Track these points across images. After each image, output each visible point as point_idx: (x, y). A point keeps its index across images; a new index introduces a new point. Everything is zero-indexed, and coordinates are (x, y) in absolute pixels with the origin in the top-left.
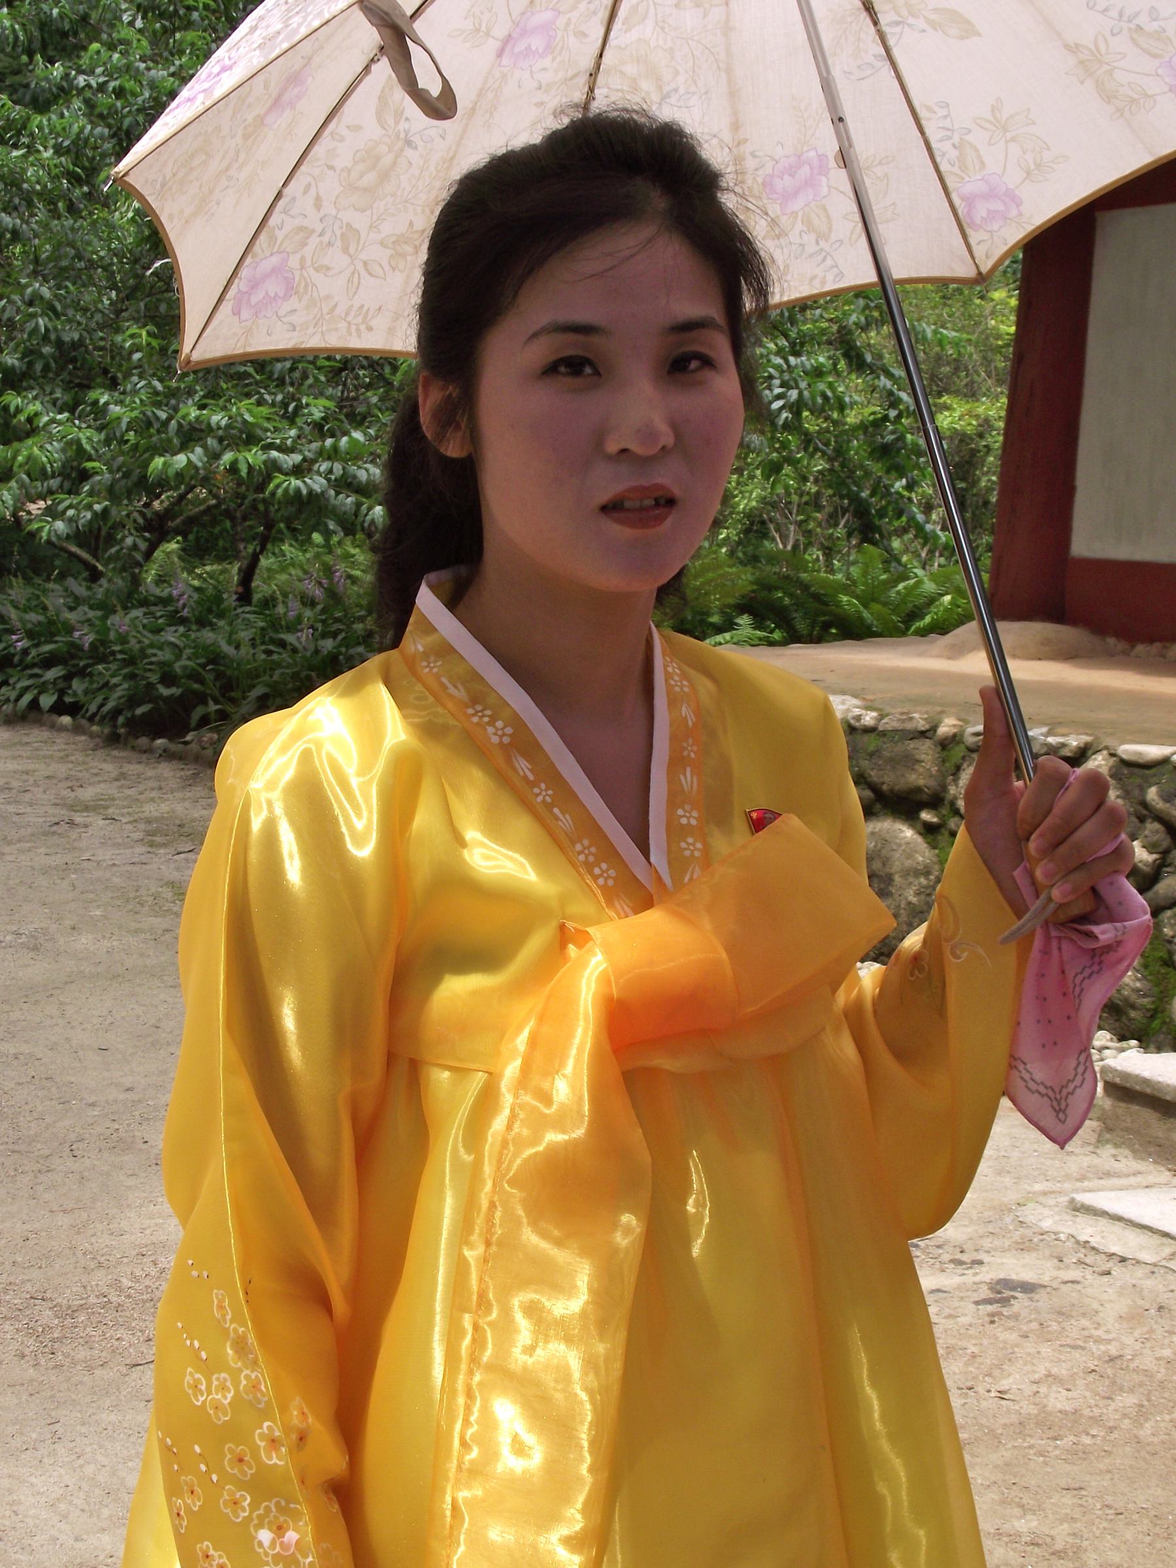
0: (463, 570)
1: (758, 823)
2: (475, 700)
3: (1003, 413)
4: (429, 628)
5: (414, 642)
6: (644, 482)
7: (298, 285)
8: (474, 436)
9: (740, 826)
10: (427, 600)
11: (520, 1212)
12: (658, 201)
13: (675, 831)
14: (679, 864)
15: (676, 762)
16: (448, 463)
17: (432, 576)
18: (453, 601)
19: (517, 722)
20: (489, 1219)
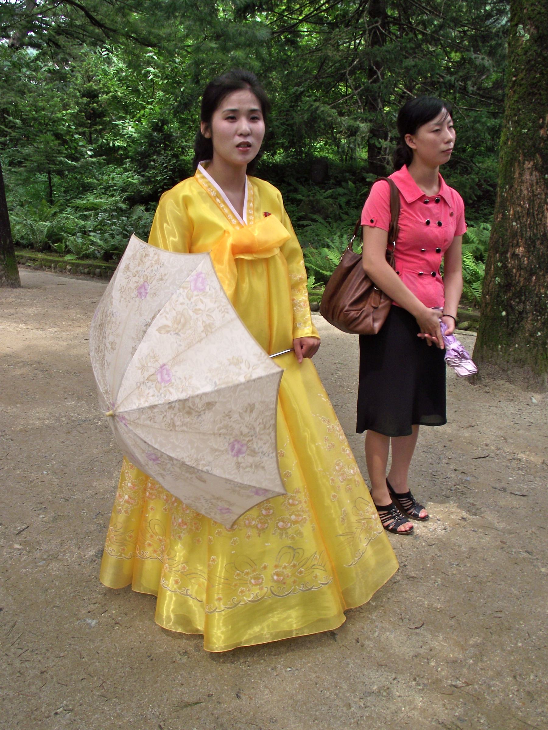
0: (208, 161)
1: (266, 215)
2: (209, 187)
3: (194, 144)
4: (200, 173)
5: (197, 175)
6: (245, 141)
7: (516, 276)
8: (211, 133)
9: (262, 215)
10: (200, 167)
11: (167, 598)
12: (248, 87)
13: (249, 214)
14: (249, 221)
15: (249, 201)
16: (206, 139)
17: (201, 162)
18: (205, 168)
19: (217, 192)
20: (224, 203)
